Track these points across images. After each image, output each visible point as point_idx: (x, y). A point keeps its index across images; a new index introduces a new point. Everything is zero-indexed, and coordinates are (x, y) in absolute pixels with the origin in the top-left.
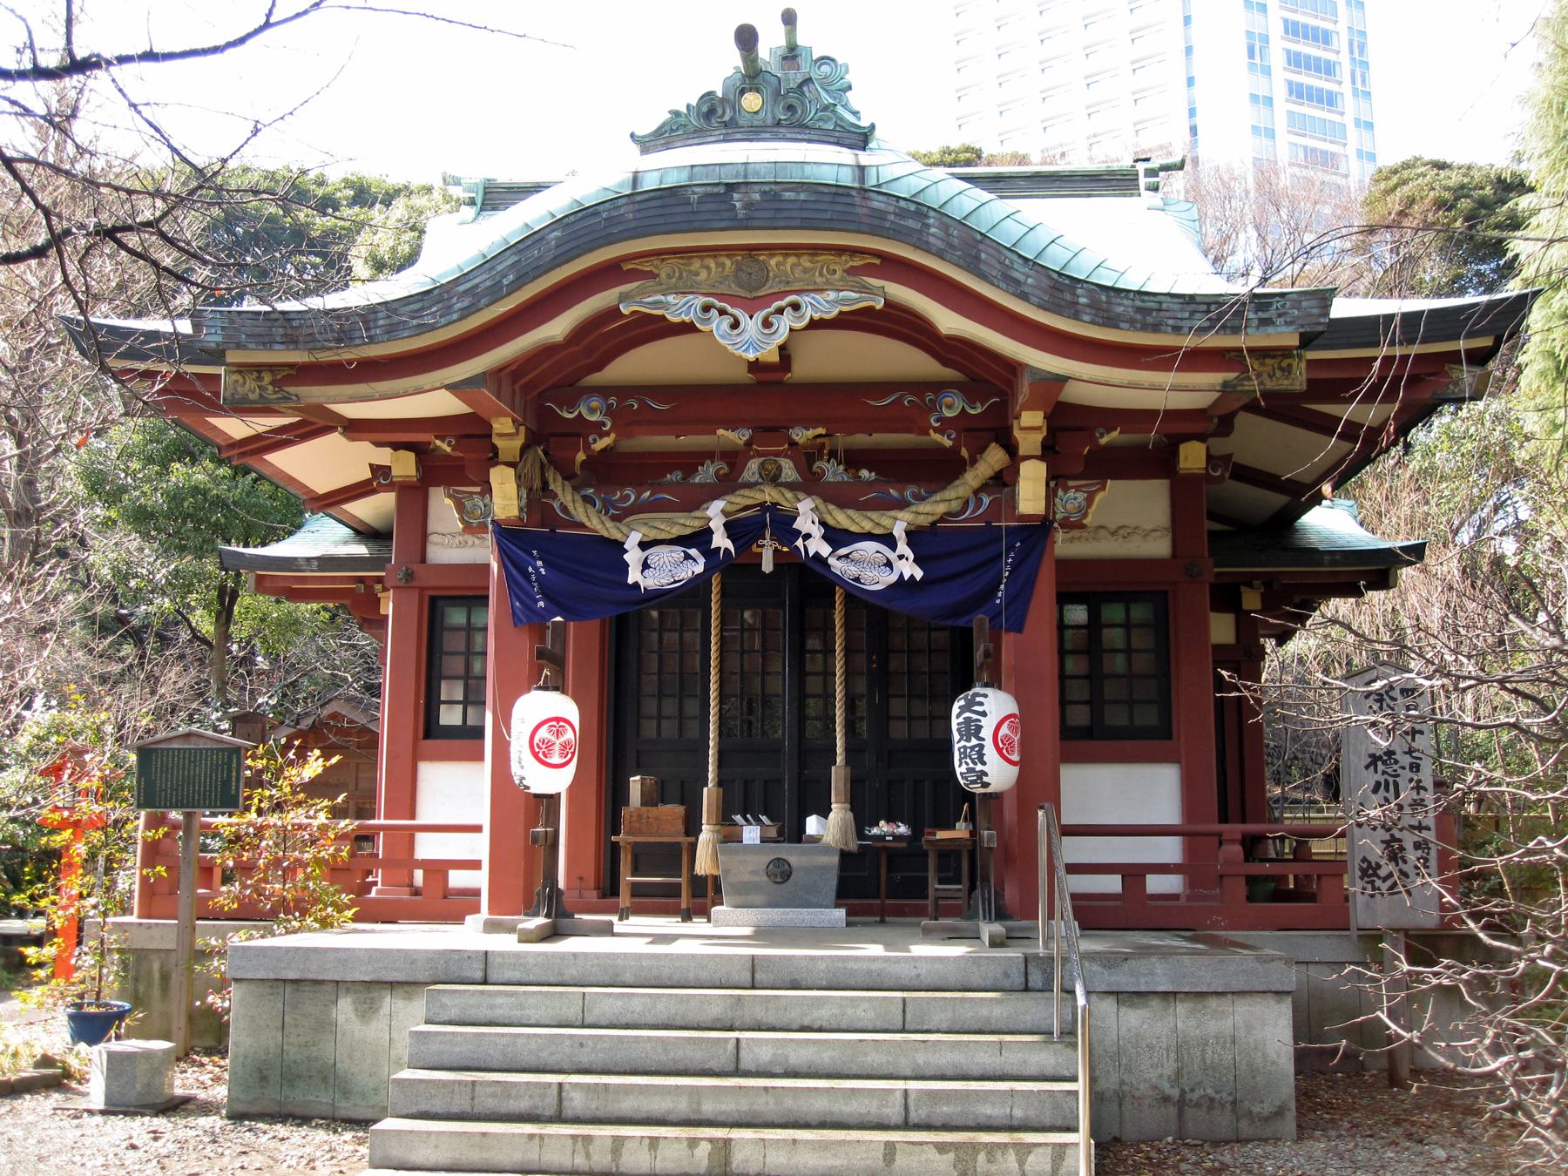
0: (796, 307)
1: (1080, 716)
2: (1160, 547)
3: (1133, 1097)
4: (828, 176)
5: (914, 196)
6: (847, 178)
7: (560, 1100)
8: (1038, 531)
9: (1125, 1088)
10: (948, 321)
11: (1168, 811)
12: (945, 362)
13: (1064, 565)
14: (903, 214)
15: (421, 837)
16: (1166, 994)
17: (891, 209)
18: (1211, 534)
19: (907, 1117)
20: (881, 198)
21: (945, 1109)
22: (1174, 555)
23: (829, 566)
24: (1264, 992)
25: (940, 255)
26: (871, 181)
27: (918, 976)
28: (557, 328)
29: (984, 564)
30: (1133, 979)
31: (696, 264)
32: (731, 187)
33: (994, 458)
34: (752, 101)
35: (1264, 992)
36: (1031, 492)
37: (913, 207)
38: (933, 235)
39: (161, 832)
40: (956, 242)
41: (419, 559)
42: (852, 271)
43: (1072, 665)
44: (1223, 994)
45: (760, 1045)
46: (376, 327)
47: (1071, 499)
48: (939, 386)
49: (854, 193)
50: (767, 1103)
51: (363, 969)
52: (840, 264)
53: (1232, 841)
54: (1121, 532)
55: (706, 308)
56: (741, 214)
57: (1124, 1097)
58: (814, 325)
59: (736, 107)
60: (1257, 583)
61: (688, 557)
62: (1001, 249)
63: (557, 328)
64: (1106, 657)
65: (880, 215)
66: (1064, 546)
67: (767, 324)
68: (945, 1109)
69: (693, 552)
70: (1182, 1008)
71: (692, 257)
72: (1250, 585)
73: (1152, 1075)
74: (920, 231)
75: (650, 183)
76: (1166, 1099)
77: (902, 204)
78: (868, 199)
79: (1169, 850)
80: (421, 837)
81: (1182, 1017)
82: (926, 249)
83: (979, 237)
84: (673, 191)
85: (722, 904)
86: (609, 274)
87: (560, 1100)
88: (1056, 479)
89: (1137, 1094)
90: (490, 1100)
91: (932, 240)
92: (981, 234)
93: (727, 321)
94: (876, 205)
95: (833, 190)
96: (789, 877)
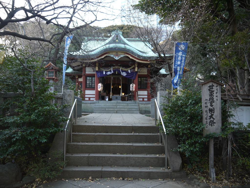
1: (139, 87)
2: (146, 74)
4: (123, 47)
6: (124, 47)
8: (137, 72)
10: (131, 58)
11: (146, 94)
13: (138, 75)
14: (128, 50)
15: (86, 95)
26: (126, 48)
28: (103, 57)
29: (133, 74)
31: (113, 53)
32: (116, 48)
33: (133, 66)
34: (117, 40)
36: (136, 70)
42: (124, 54)
43: (139, 83)
47: (139, 70)
52: (123, 53)
55: (114, 56)
59: (116, 41)
63: (103, 57)
65: (126, 50)
66: (139, 73)
67: (118, 57)
70: (146, 105)
71: (110, 51)
73: (144, 109)
75: (110, 47)
76: (144, 111)
79: (146, 97)
80: (86, 95)
81: (146, 106)
82: (129, 52)
84: (112, 48)
85: (131, 79)
86: (106, 53)
88: (138, 69)
93: (115, 57)
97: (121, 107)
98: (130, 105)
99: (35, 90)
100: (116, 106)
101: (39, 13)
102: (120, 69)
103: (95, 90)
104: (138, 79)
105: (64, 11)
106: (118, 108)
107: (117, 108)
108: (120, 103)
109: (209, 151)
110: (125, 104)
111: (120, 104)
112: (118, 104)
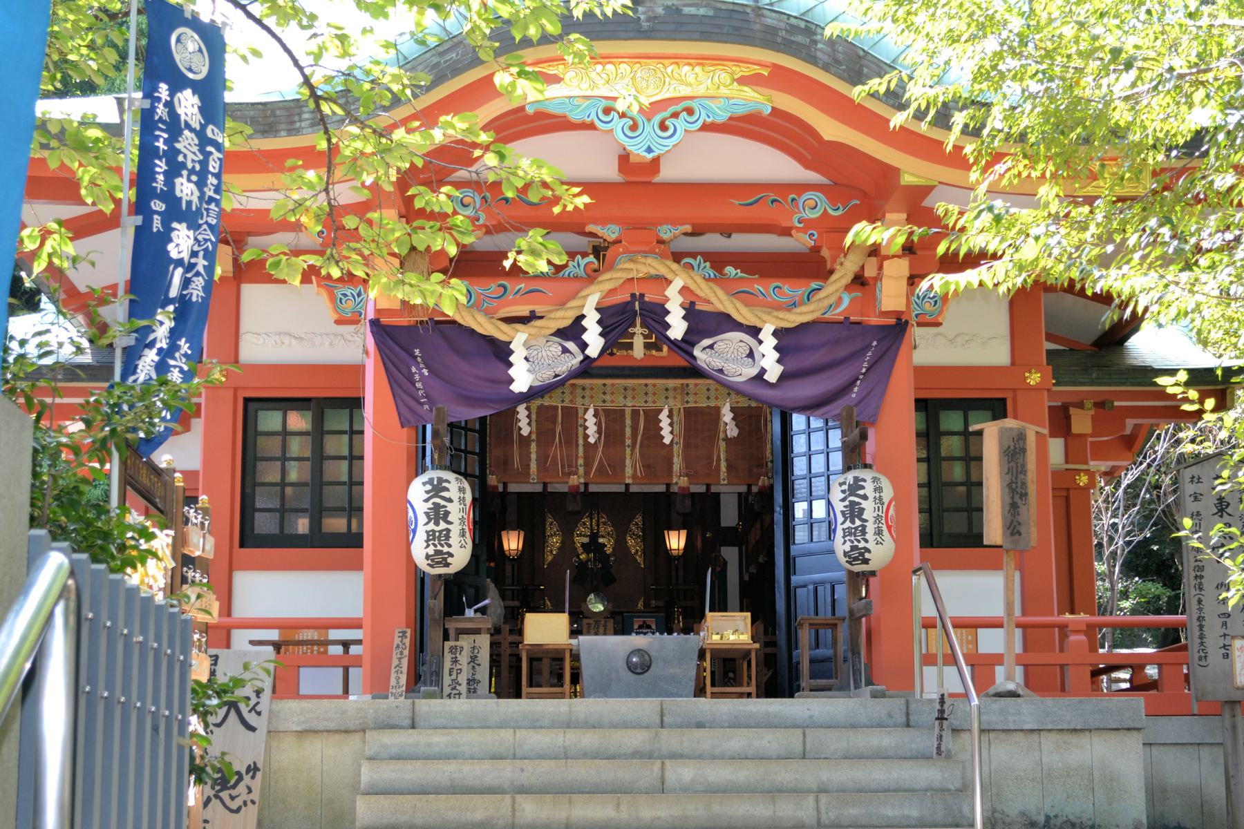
0: (690, 111)
3: (1004, 823)
5: (803, 14)
7: (514, 810)
9: (997, 815)
12: (807, 165)
14: (793, 29)
16: (1032, 731)
17: (782, 25)
18: (1049, 352)
19: (819, 820)
20: (774, 15)
21: (851, 811)
22: (1013, 363)
23: (695, 358)
24: (1117, 729)
25: (826, 68)
27: (811, 717)
30: (1002, 718)
35: (1117, 729)
37: (802, 25)
38: (821, 50)
39: (1138, 160)
40: (840, 57)
41: (233, 359)
44: (1082, 730)
45: (682, 773)
46: (300, 121)
48: (802, 188)
49: (749, 10)
50: (697, 809)
51: (296, 719)
53: (1077, 632)
54: (959, 339)
56: (645, 25)
57: (996, 822)
58: (706, 127)
60: (1089, 404)
61: (565, 350)
62: (882, 65)
64: (944, 465)
65: (772, 31)
67: (663, 127)
68: (851, 811)
69: (571, 345)
70: (1048, 741)
72: (1081, 405)
74: (808, 47)
77: (793, 21)
78: (762, 16)
81: (1052, 752)
82: (812, 60)
83: (862, 53)
87: (514, 810)
89: (1008, 820)
90: (450, 812)
91: (819, 55)
92: (864, 50)
94: (769, 21)
95: (731, 7)
96: (649, 667)
97: (718, 773)
98: (836, 742)
99: (754, 331)
100: (650, 756)
101: (47, 300)
102: (678, 284)
103: (358, 566)
104: (777, 406)
105: (235, 808)
106: (687, 790)
107: (661, 788)
108: (700, 725)
109: (556, 647)
110: (769, 741)
111: (704, 740)
112: (671, 740)
